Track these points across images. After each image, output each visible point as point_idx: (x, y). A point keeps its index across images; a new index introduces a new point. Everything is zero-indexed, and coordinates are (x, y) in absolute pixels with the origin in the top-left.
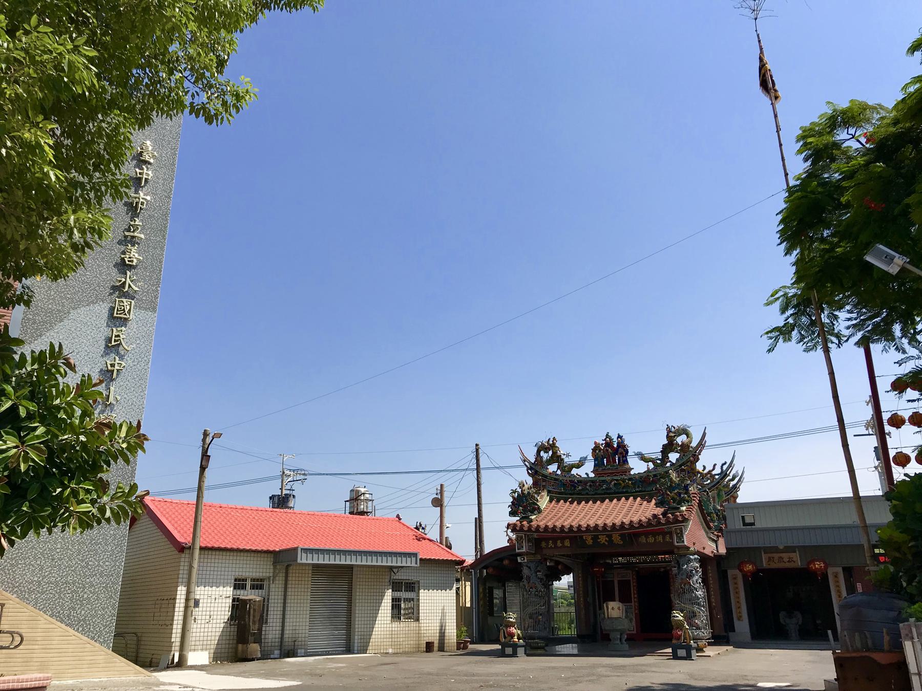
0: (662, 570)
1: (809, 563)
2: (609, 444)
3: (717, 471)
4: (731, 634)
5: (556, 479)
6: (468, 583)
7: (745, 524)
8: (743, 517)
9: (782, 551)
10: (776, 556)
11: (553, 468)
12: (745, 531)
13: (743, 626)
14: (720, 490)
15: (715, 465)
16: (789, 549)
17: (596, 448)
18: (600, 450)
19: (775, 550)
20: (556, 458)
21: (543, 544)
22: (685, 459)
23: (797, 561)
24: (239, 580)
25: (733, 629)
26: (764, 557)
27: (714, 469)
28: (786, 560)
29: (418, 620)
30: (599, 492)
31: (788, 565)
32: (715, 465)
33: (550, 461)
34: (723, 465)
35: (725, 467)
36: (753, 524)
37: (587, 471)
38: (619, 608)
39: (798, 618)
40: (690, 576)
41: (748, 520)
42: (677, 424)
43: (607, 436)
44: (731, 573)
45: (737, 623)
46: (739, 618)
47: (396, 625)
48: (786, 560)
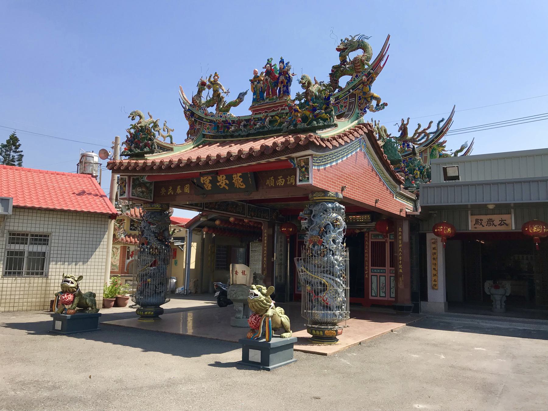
0: (358, 231)
1: (526, 225)
2: (269, 72)
3: (433, 128)
4: (423, 303)
5: (211, 121)
6: (194, 245)
7: (447, 178)
8: (445, 170)
9: (493, 212)
10: (485, 218)
11: (212, 110)
12: (447, 186)
13: (437, 295)
14: (434, 149)
15: (431, 122)
16: (502, 208)
17: (255, 80)
18: (260, 81)
19: (481, 209)
20: (217, 99)
21: (163, 190)
22: (357, 80)
23: (511, 224)
24: (14, 234)
25: (425, 297)
26: (471, 220)
27: (429, 127)
28: (497, 222)
29: (47, 276)
30: (252, 131)
31: (503, 229)
32: (431, 122)
33: (210, 103)
34: (439, 122)
35: (442, 124)
36: (457, 178)
37: (243, 111)
38: (243, 273)
39: (508, 287)
40: (324, 231)
41: (451, 172)
42: (350, 32)
43: (269, 62)
44: (430, 237)
45: (430, 292)
46: (434, 287)
47: (9, 280)
48: (497, 222)
